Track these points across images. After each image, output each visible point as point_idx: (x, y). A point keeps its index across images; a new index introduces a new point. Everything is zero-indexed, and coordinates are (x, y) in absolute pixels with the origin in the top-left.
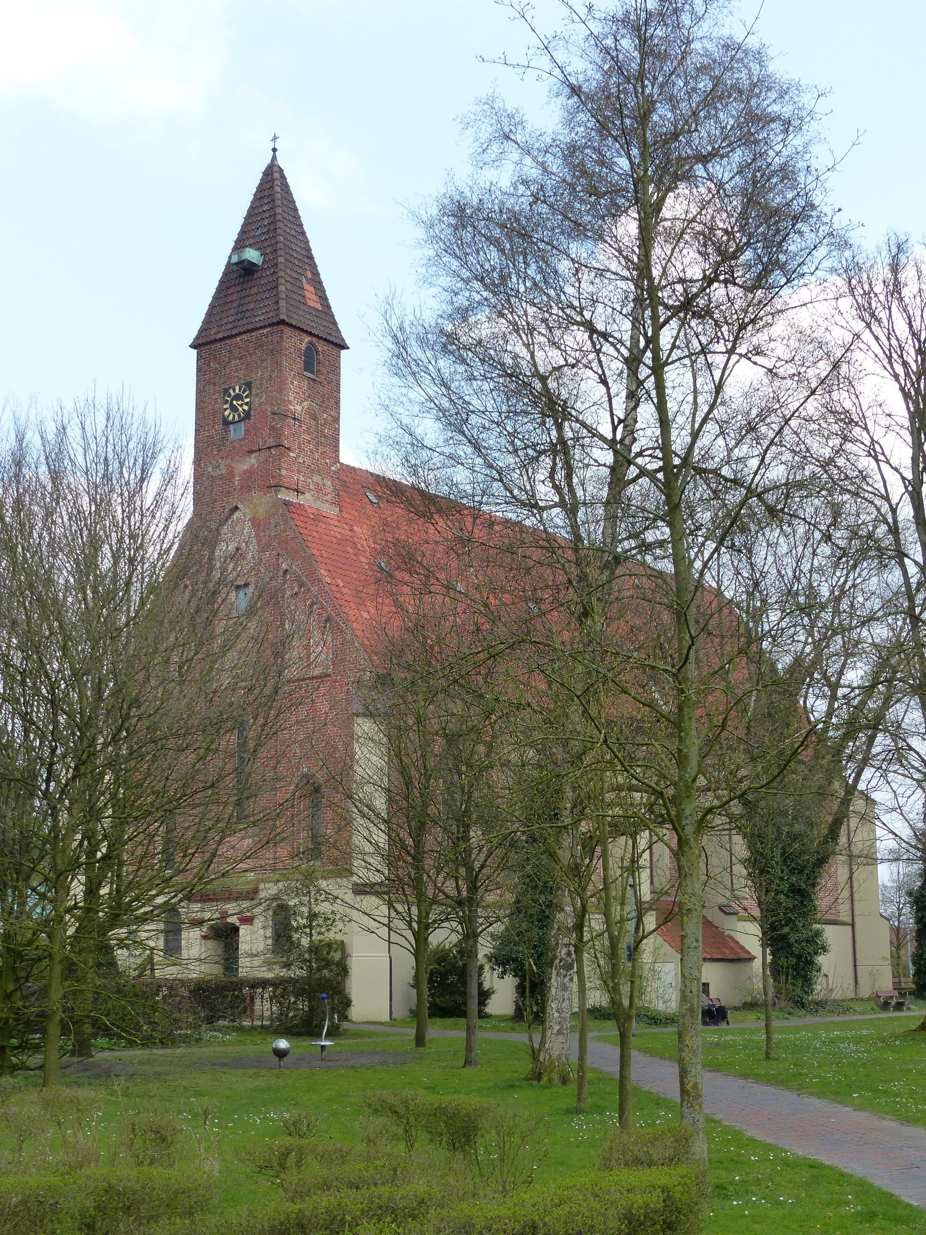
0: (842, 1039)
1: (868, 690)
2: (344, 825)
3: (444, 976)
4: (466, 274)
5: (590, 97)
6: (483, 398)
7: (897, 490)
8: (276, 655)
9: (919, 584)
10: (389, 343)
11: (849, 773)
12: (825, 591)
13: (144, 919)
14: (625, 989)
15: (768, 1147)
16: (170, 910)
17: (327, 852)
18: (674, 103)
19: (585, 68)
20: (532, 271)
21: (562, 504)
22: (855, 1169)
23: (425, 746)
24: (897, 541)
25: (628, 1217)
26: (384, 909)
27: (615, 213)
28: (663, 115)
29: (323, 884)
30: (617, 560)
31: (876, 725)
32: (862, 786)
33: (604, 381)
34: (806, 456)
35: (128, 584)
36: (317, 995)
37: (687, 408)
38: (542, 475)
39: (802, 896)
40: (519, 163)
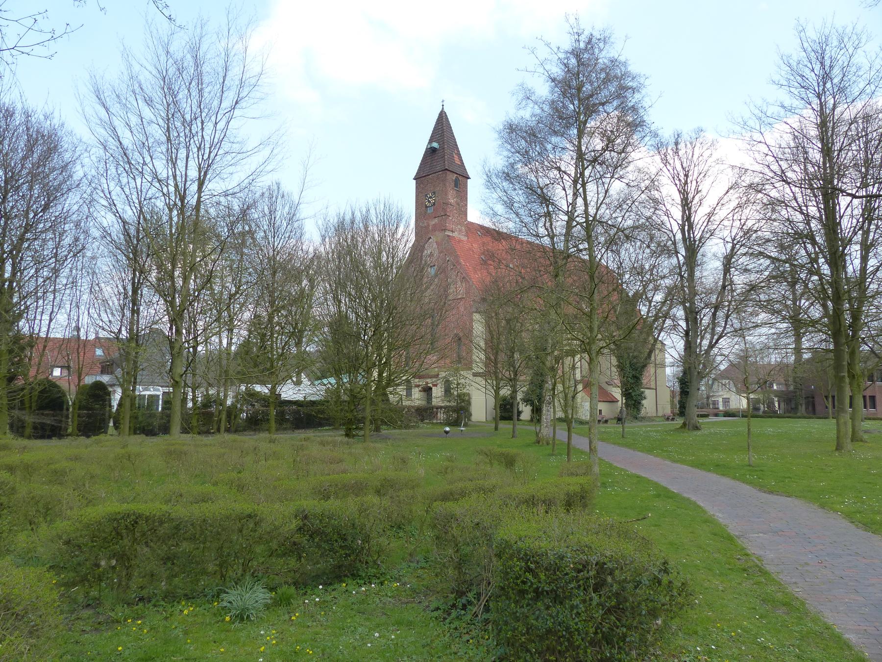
0: (651, 431)
1: (663, 303)
2: (470, 352)
3: (505, 406)
4: (513, 150)
5: (559, 82)
6: (519, 197)
7: (676, 228)
8: (445, 291)
9: (684, 263)
10: (485, 177)
11: (656, 333)
12: (647, 267)
13: (398, 385)
14: (570, 412)
15: (622, 470)
16: (408, 381)
17: (463, 362)
18: (592, 84)
19: (557, 71)
20: (537, 149)
21: (548, 235)
22: (654, 478)
23: (498, 324)
24: (675, 247)
25: (568, 494)
26: (484, 382)
27: (568, 127)
28: (587, 88)
29: (462, 373)
30: (569, 256)
31: (666, 316)
32: (660, 339)
33: (564, 189)
34: (639, 215)
35: (392, 266)
36: (460, 411)
37: (595, 199)
38: (541, 224)
39: (637, 379)
40: (533, 108)
